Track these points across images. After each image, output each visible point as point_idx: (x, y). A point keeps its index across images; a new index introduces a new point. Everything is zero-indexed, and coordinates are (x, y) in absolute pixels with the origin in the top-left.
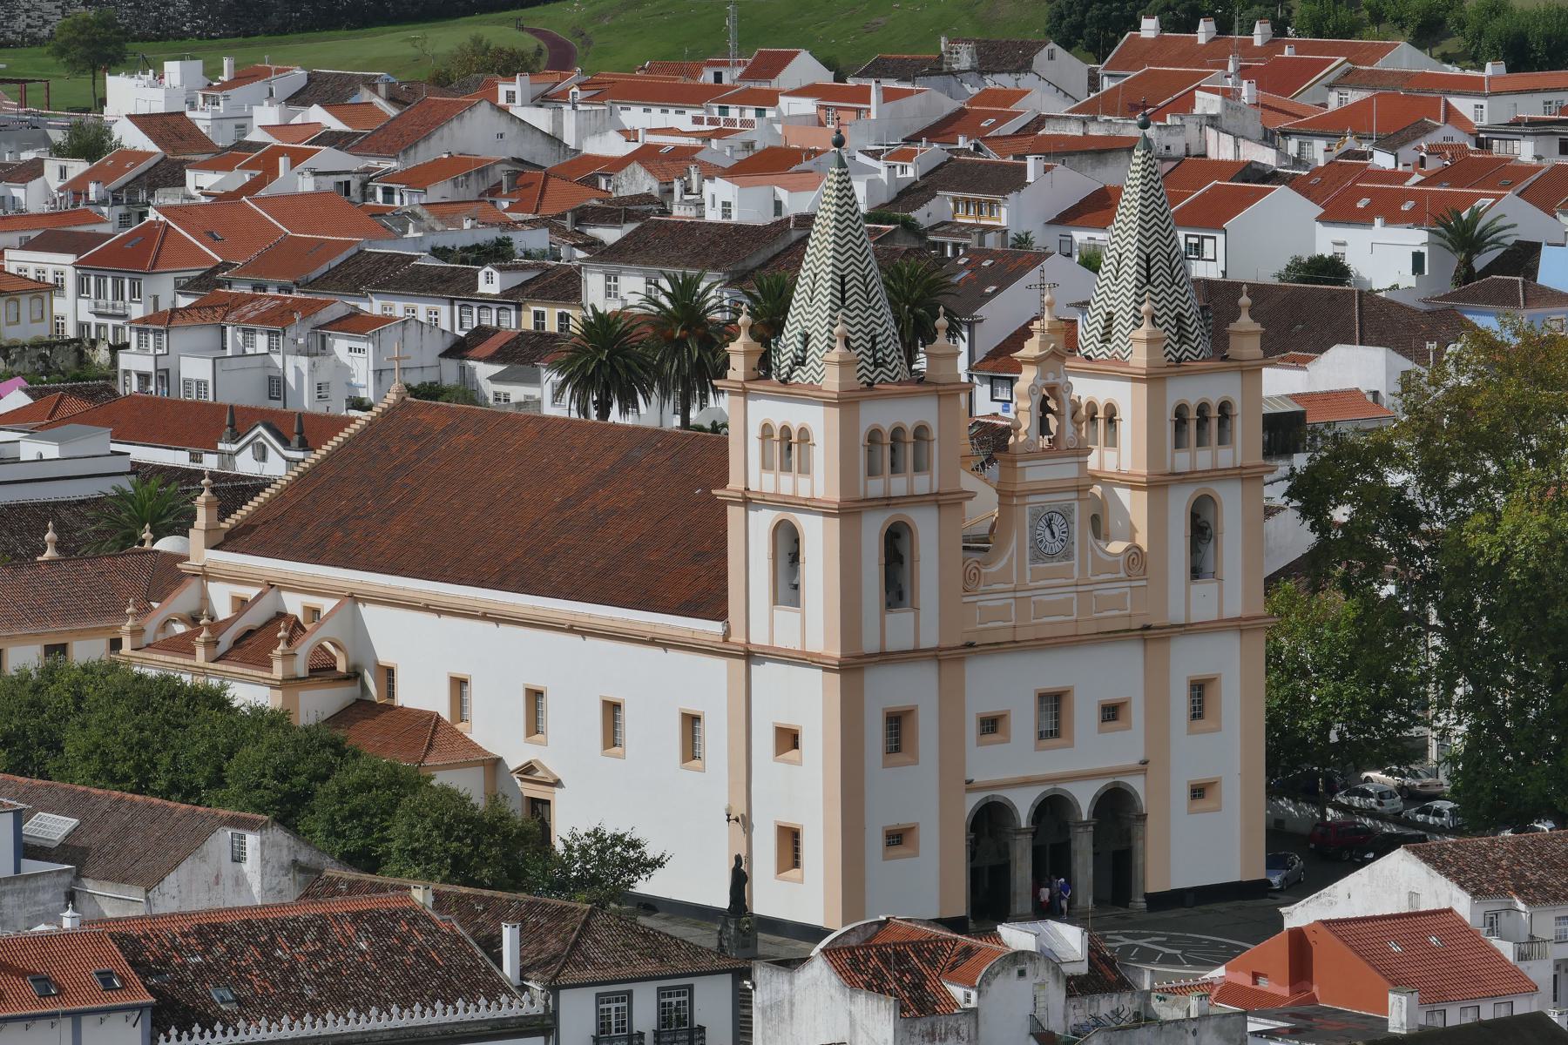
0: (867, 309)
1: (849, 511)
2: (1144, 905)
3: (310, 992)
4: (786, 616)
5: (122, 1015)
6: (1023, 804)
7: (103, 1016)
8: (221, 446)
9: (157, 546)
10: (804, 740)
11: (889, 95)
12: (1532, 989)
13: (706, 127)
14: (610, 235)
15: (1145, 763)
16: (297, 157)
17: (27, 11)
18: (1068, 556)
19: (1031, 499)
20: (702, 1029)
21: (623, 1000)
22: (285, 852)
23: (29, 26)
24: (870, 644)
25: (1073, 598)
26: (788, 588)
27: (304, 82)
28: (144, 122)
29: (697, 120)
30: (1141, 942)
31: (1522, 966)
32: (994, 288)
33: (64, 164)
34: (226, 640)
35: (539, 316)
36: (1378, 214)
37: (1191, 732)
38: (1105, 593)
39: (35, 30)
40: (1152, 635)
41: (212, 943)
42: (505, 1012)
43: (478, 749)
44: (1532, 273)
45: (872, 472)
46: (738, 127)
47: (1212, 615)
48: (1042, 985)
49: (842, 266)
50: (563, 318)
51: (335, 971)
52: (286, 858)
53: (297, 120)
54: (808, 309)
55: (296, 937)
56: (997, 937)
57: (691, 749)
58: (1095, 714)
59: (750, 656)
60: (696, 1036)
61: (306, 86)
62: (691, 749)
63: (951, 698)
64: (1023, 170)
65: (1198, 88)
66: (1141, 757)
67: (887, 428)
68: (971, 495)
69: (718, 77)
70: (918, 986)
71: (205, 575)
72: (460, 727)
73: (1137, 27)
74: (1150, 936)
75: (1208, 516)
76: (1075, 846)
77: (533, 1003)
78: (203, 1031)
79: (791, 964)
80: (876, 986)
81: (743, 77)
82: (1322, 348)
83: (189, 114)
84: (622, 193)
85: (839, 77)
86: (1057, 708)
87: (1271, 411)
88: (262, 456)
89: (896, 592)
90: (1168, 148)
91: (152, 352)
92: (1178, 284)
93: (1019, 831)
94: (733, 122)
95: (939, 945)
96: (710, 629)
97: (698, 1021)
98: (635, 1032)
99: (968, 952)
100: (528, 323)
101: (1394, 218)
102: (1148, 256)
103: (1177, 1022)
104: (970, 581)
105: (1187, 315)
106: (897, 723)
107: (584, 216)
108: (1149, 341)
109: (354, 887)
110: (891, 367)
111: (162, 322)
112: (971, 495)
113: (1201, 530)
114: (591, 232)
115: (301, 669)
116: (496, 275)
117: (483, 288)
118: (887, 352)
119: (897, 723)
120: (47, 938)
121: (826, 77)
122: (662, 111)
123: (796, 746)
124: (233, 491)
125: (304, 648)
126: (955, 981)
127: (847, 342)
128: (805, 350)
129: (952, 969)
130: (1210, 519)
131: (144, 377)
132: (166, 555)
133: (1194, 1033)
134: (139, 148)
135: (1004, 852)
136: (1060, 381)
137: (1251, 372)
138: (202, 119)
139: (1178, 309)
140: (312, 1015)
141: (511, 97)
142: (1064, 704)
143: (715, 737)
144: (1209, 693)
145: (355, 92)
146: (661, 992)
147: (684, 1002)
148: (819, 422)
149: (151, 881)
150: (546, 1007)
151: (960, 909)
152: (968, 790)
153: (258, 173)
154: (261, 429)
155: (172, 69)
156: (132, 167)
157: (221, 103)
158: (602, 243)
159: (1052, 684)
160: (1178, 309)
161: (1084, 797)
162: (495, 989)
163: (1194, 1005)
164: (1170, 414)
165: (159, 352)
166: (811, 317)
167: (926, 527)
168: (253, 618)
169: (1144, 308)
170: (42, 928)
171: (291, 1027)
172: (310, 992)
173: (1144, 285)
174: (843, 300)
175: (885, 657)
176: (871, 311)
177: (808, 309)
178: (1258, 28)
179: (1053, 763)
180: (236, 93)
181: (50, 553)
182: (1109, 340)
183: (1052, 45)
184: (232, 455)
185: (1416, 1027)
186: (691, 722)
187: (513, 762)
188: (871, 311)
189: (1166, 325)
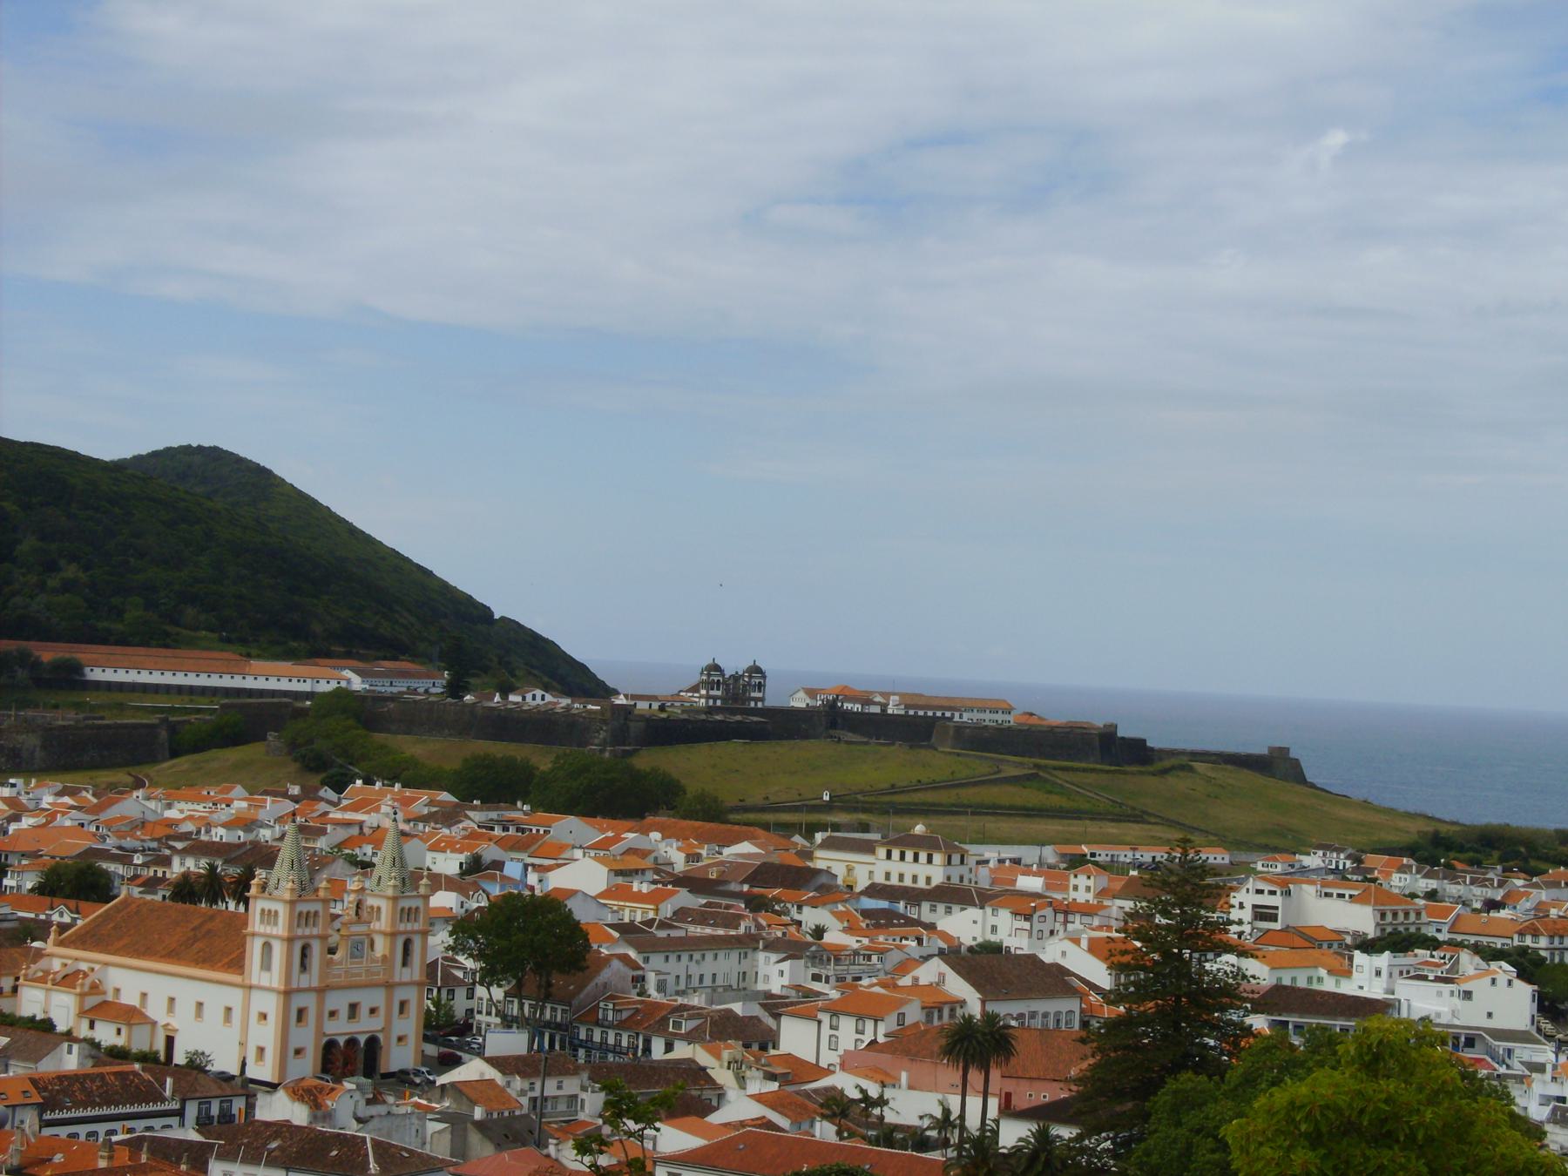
1: (290, 940)
3: (97, 1100)
4: (265, 975)
5: (29, 1107)
8: (47, 912)
10: (268, 1017)
11: (273, 802)
13: (207, 810)
14: (179, 845)
16: (64, 814)
18: (362, 957)
19: (353, 937)
24: (294, 986)
26: (266, 965)
34: (59, 977)
35: (156, 871)
37: (296, 1026)
40: (389, 986)
41: (63, 1082)
42: (167, 1107)
45: (298, 926)
47: (268, 985)
48: (357, 1101)
50: (164, 872)
51: (106, 1092)
52: (87, 1052)
53: (59, 801)
55: (93, 1081)
56: (343, 1085)
58: (367, 1012)
59: (251, 987)
63: (321, 1003)
64: (326, 829)
67: (407, 907)
68: (331, 936)
69: (208, 793)
70: (315, 1100)
71: (51, 955)
72: (144, 1010)
73: (355, 783)
77: (175, 1106)
80: (301, 1099)
84: (180, 831)
88: (61, 915)
89: (304, 967)
96: (236, 979)
99: (333, 1089)
100: (152, 874)
101: (454, 851)
103: (403, 1115)
104: (330, 963)
106: (301, 1013)
107: (169, 837)
112: (331, 936)
114: (171, 843)
115: (86, 989)
116: (141, 857)
117: (135, 861)
119: (301, 1013)
121: (247, 795)
125: (88, 981)
127: (395, 878)
128: (278, 884)
131: (12, 888)
132: (36, 948)
136: (364, 898)
137: (426, 898)
138: (24, 799)
142: (358, 1007)
143: (237, 1015)
144: (406, 1007)
145: (80, 792)
146: (221, 1102)
148: (282, 910)
149: (37, 1060)
159: (354, 1000)
161: (362, 1039)
163: (409, 1109)
167: (317, 949)
168: (68, 971)
169: (393, 874)
172: (97, 1100)
175: (299, 990)
178: (397, 785)
180: (36, 791)
183: (326, 788)
184: (51, 915)
186: (229, 1010)
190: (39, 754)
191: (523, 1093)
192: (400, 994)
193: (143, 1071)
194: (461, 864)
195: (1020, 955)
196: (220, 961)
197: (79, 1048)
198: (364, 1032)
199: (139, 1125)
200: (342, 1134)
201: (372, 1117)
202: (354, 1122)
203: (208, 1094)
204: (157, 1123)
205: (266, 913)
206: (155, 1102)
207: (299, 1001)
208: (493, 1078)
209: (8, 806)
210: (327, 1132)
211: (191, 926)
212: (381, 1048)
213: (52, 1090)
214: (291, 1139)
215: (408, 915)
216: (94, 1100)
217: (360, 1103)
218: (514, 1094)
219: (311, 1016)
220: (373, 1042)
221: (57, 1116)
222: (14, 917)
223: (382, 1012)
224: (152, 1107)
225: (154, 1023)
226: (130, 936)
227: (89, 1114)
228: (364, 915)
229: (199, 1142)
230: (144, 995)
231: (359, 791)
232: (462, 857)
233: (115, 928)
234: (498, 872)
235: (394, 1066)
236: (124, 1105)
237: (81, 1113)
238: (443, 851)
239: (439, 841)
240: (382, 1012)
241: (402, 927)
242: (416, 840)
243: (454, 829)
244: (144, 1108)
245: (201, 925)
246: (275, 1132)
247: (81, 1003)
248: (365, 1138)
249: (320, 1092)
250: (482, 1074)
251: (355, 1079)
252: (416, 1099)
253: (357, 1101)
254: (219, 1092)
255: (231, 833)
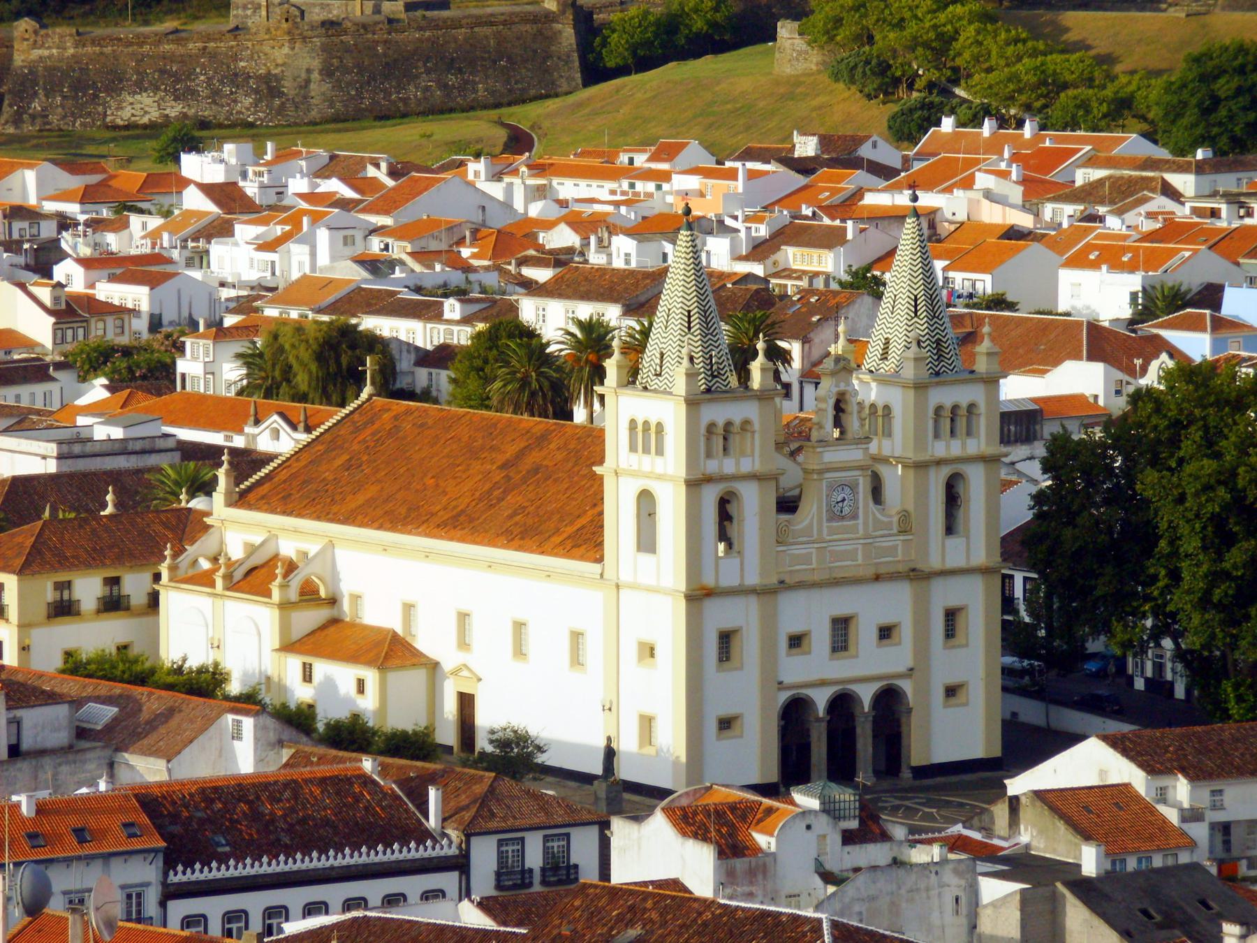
0: (707, 335)
1: (694, 484)
2: (911, 775)
5: (141, 857)
6: (821, 699)
7: (126, 857)
9: (190, 505)
12: (1192, 845)
13: (618, 198)
15: (911, 669)
17: (132, 104)
19: (827, 475)
20: (576, 866)
21: (563, 840)
22: (271, 734)
23: (133, 115)
25: (857, 549)
27: (327, 160)
28: (209, 190)
29: (613, 192)
30: (907, 803)
31: (1186, 827)
32: (818, 317)
33: (144, 220)
34: (238, 575)
36: (1106, 262)
38: (884, 544)
39: (137, 118)
40: (917, 576)
42: (430, 853)
43: (421, 655)
44: (1216, 305)
45: (709, 455)
46: (642, 198)
48: (823, 837)
49: (689, 304)
52: (272, 736)
54: (664, 335)
57: (576, 660)
58: (874, 634)
60: (572, 871)
61: (327, 165)
62: (576, 660)
65: (979, 170)
66: (910, 664)
67: (721, 423)
70: (733, 833)
73: (938, 123)
74: (914, 798)
75: (960, 489)
76: (859, 731)
77: (448, 850)
78: (203, 867)
79: (638, 817)
81: (650, 160)
82: (1057, 362)
83: (241, 184)
85: (720, 162)
86: (846, 629)
87: (1006, 410)
88: (276, 434)
90: (954, 214)
91: (201, 359)
92: (938, 317)
93: (818, 720)
94: (638, 194)
95: (751, 808)
97: (573, 861)
98: (526, 868)
99: (770, 811)
101: (1117, 266)
102: (916, 296)
105: (944, 340)
108: (916, 360)
109: (322, 759)
110: (724, 378)
111: (158, 351)
113: (952, 499)
115: (293, 595)
116: (458, 305)
117: (447, 315)
118: (721, 367)
119: (726, 638)
120: (86, 799)
122: (588, 185)
123: (652, 655)
124: (246, 462)
125: (296, 581)
126: (761, 831)
129: (757, 823)
130: (961, 494)
133: (937, 873)
134: (202, 209)
135: (806, 734)
137: (992, 382)
138: (251, 189)
139: (938, 336)
140: (285, 855)
141: (477, 174)
143: (594, 649)
144: (960, 621)
146: (546, 839)
147: (563, 846)
150: (460, 847)
151: (773, 776)
152: (780, 689)
153: (288, 228)
154: (276, 417)
155: (229, 147)
156: (195, 222)
157: (266, 175)
158: (536, 282)
159: (842, 611)
160: (938, 336)
161: (866, 694)
162: (423, 835)
164: (931, 413)
165: (207, 360)
166: (665, 341)
170: (84, 790)
171: (269, 864)
173: (913, 318)
174: (689, 328)
176: (709, 336)
177: (664, 335)
178: (1027, 125)
179: (841, 669)
181: (109, 510)
182: (886, 358)
185: (1103, 872)
187: (447, 665)
188: (709, 336)
189: (928, 348)
190: (319, 88)
191: (1193, 815)
192: (945, 594)
193: (380, 774)
194: (1134, 296)
195: (427, 795)
196: (557, 531)
197: (255, 726)
198: (823, 683)
199: (374, 890)
200: (769, 914)
201: (857, 870)
202: (818, 881)
203: (518, 823)
204: (412, 885)
205: (880, 413)
206: (404, 843)
207: (721, 615)
208: (1126, 781)
209: (218, 202)
210: (737, 908)
211: (501, 459)
212: (910, 711)
213: (190, 818)
214: (664, 924)
215: (936, 421)
216: (278, 840)
217: (828, 841)
218: (1172, 815)
219: (749, 647)
220: (889, 699)
221: (198, 876)
222: (170, 443)
223: (906, 633)
224: (397, 854)
225: (434, 666)
226: (379, 481)
227: (265, 869)
228: (853, 423)
229: (477, 931)
230: (408, 608)
231: (952, 142)
232: (1134, 282)
233: (348, 466)
234: (1208, 312)
235: (943, 753)
236: (339, 849)
237: (249, 869)
238: (1095, 265)
239: (1089, 248)
240: (906, 633)
241: (940, 449)
242: (1035, 248)
243: (1131, 217)
244: (381, 855)
245: (520, 455)
246: (632, 909)
247: (285, 627)
248: (820, 921)
249: (744, 818)
250: (1102, 773)
251: (817, 785)
252: (958, 829)
253: (823, 837)
254: (541, 818)
255: (651, 247)
